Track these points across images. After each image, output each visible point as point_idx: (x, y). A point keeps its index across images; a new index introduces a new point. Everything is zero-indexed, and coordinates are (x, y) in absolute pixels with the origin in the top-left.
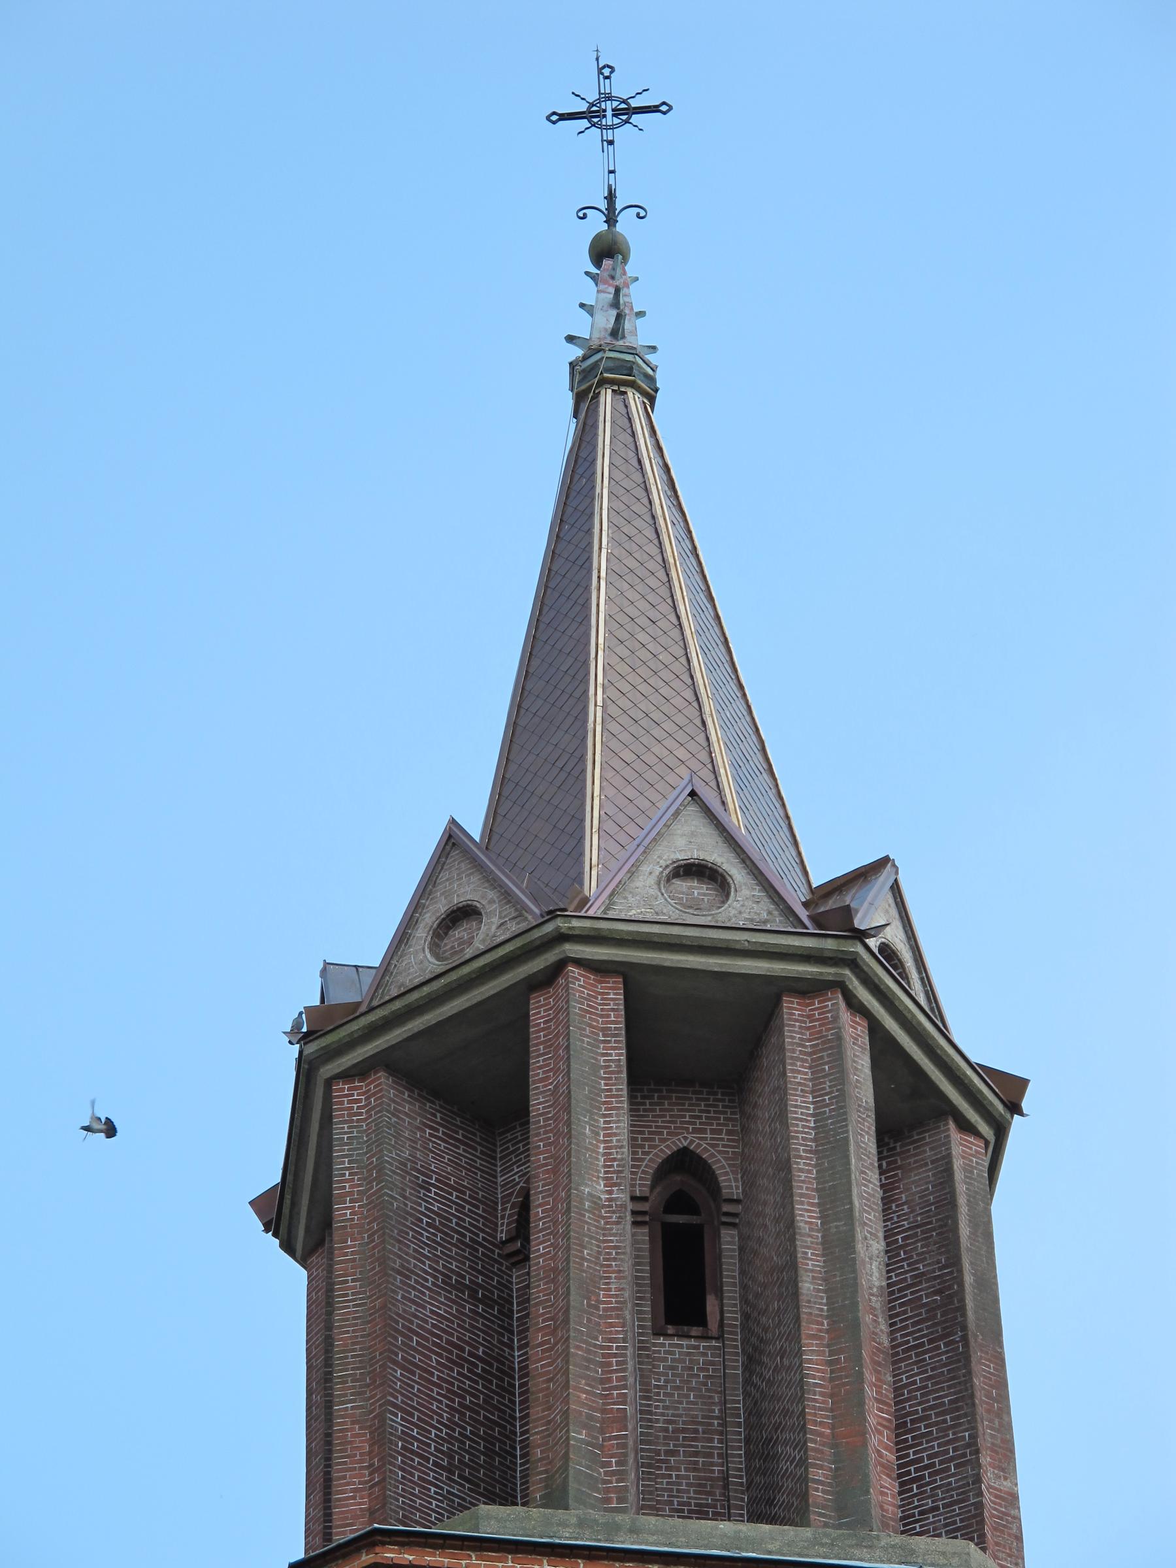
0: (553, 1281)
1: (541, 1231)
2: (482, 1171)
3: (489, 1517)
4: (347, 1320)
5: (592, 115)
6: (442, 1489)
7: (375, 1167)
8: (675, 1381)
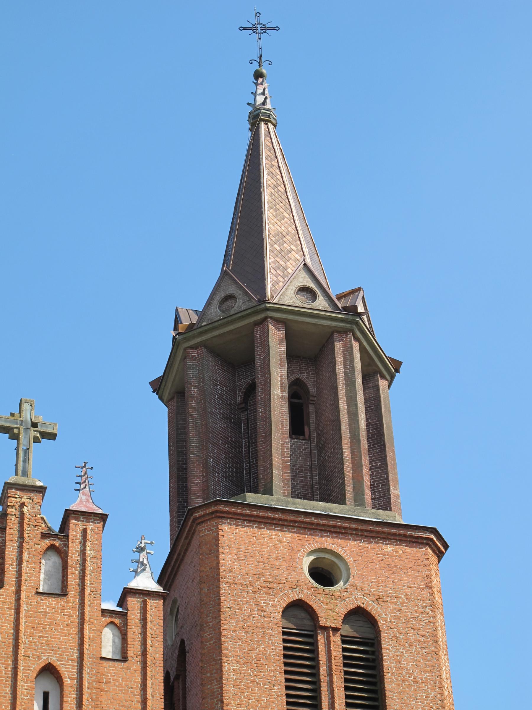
0: (265, 421)
1: (260, 404)
2: (232, 381)
3: (249, 497)
4: (194, 427)
5: (253, 29)
6: (224, 484)
7: (201, 378)
8: (295, 453)
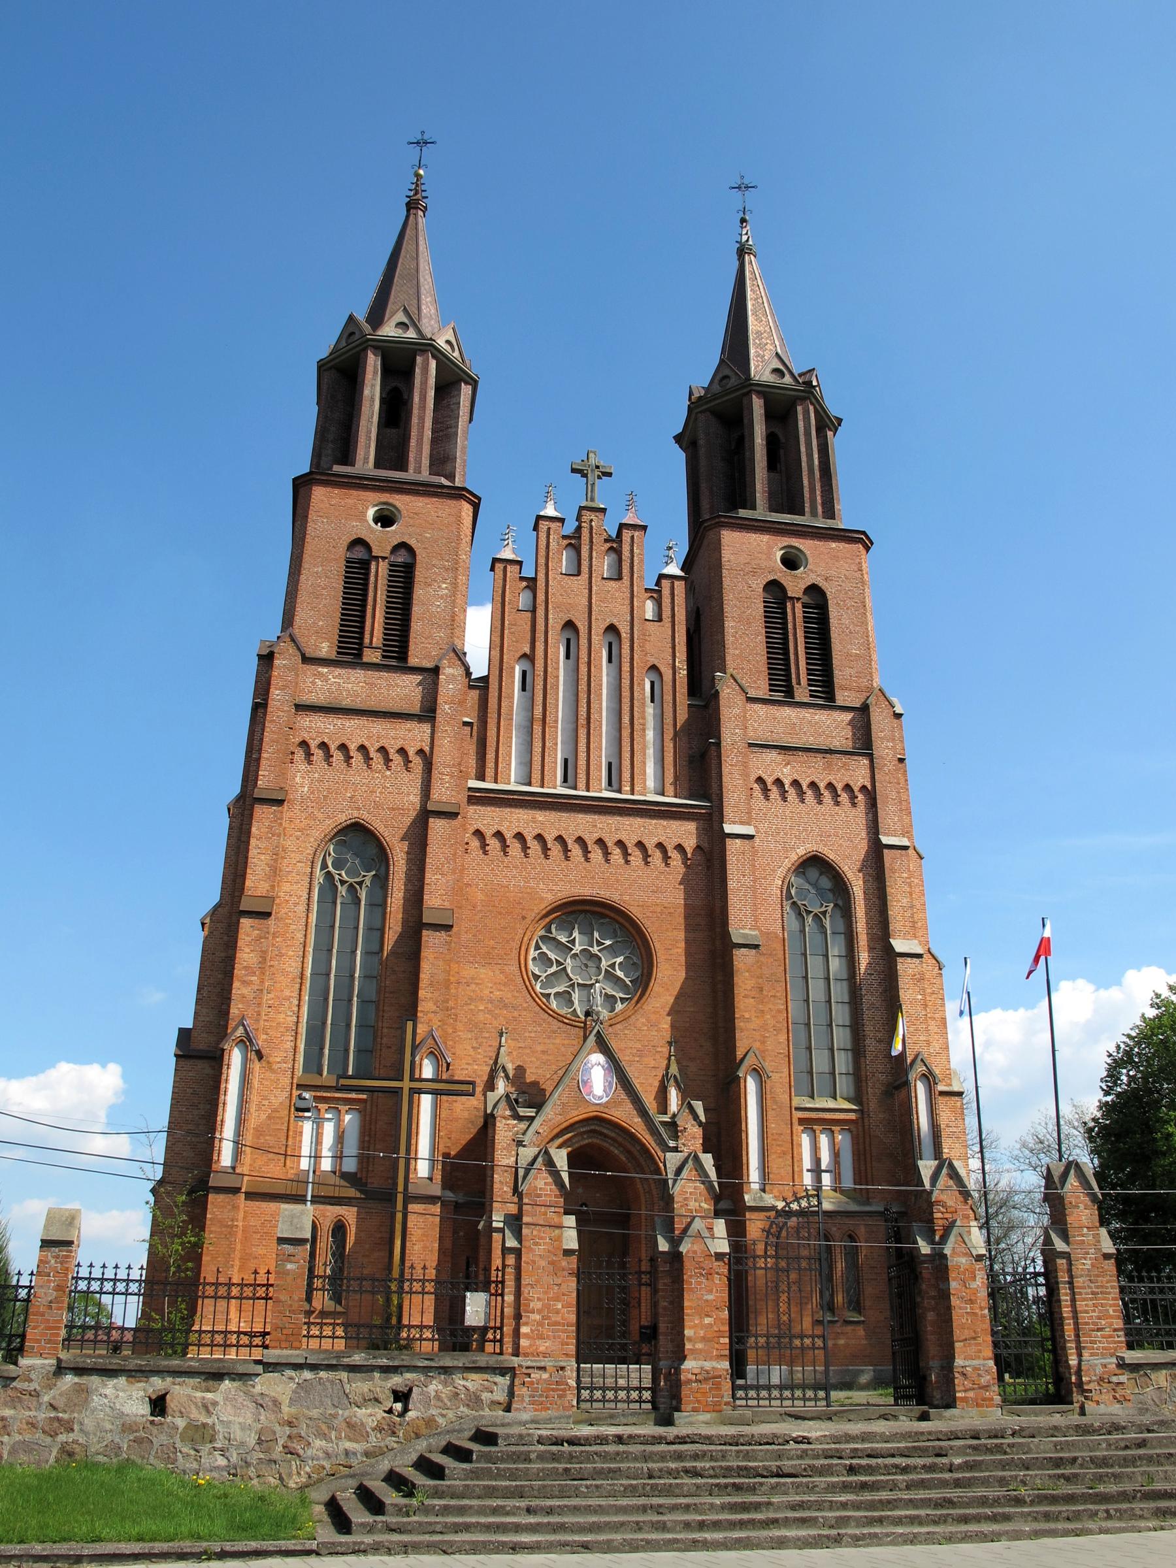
5: (739, 188)
